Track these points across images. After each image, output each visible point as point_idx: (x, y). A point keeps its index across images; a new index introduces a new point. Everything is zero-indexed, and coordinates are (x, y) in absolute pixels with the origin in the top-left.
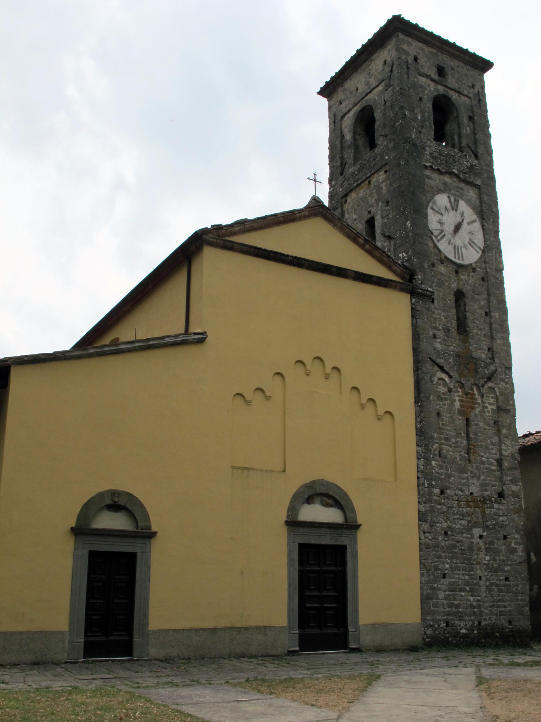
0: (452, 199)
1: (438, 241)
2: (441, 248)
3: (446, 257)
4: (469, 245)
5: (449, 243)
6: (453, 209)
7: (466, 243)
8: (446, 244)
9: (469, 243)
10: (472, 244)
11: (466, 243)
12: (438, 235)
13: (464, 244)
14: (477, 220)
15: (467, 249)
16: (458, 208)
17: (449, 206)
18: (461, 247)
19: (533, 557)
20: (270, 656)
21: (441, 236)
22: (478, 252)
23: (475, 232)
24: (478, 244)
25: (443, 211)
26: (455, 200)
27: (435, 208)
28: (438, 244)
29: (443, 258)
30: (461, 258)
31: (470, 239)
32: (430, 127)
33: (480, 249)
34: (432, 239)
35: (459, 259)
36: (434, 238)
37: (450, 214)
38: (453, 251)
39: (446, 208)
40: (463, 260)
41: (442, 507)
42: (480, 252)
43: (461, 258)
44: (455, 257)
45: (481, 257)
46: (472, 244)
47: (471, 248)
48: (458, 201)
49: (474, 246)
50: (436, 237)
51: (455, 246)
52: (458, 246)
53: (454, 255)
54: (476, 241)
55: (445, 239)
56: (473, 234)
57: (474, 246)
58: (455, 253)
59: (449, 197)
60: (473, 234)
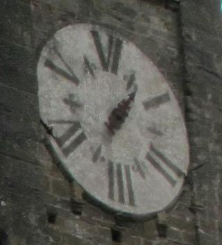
0: (104, 40)
1: (66, 152)
2: (73, 171)
3: (86, 196)
4: (148, 163)
5: (95, 159)
6: (105, 66)
10: (157, 159)
11: (142, 157)
12: (66, 137)
13: (136, 160)
14: (172, 96)
15: (143, 175)
16: (120, 63)
17: (94, 58)
18: (127, 168)
22: (173, 183)
24: (175, 162)
25: (78, 71)
26: (111, 42)
27: (57, 63)
28: (66, 161)
30: (126, 199)
31: (152, 148)
33: (179, 173)
34: (49, 147)
35: (122, 200)
36: (54, 145)
37: (99, 80)
38: (105, 179)
39: (86, 62)
40: (132, 202)
43: (126, 199)
44: (111, 195)
45: (182, 195)
46: (157, 159)
48: (119, 44)
49: (164, 166)
50: (60, 142)
51: (111, 164)
52: (119, 166)
53: (107, 190)
54: (167, 153)
56: (160, 134)
57: (164, 166)
58: (111, 185)
59: (94, 34)
60: (160, 134)
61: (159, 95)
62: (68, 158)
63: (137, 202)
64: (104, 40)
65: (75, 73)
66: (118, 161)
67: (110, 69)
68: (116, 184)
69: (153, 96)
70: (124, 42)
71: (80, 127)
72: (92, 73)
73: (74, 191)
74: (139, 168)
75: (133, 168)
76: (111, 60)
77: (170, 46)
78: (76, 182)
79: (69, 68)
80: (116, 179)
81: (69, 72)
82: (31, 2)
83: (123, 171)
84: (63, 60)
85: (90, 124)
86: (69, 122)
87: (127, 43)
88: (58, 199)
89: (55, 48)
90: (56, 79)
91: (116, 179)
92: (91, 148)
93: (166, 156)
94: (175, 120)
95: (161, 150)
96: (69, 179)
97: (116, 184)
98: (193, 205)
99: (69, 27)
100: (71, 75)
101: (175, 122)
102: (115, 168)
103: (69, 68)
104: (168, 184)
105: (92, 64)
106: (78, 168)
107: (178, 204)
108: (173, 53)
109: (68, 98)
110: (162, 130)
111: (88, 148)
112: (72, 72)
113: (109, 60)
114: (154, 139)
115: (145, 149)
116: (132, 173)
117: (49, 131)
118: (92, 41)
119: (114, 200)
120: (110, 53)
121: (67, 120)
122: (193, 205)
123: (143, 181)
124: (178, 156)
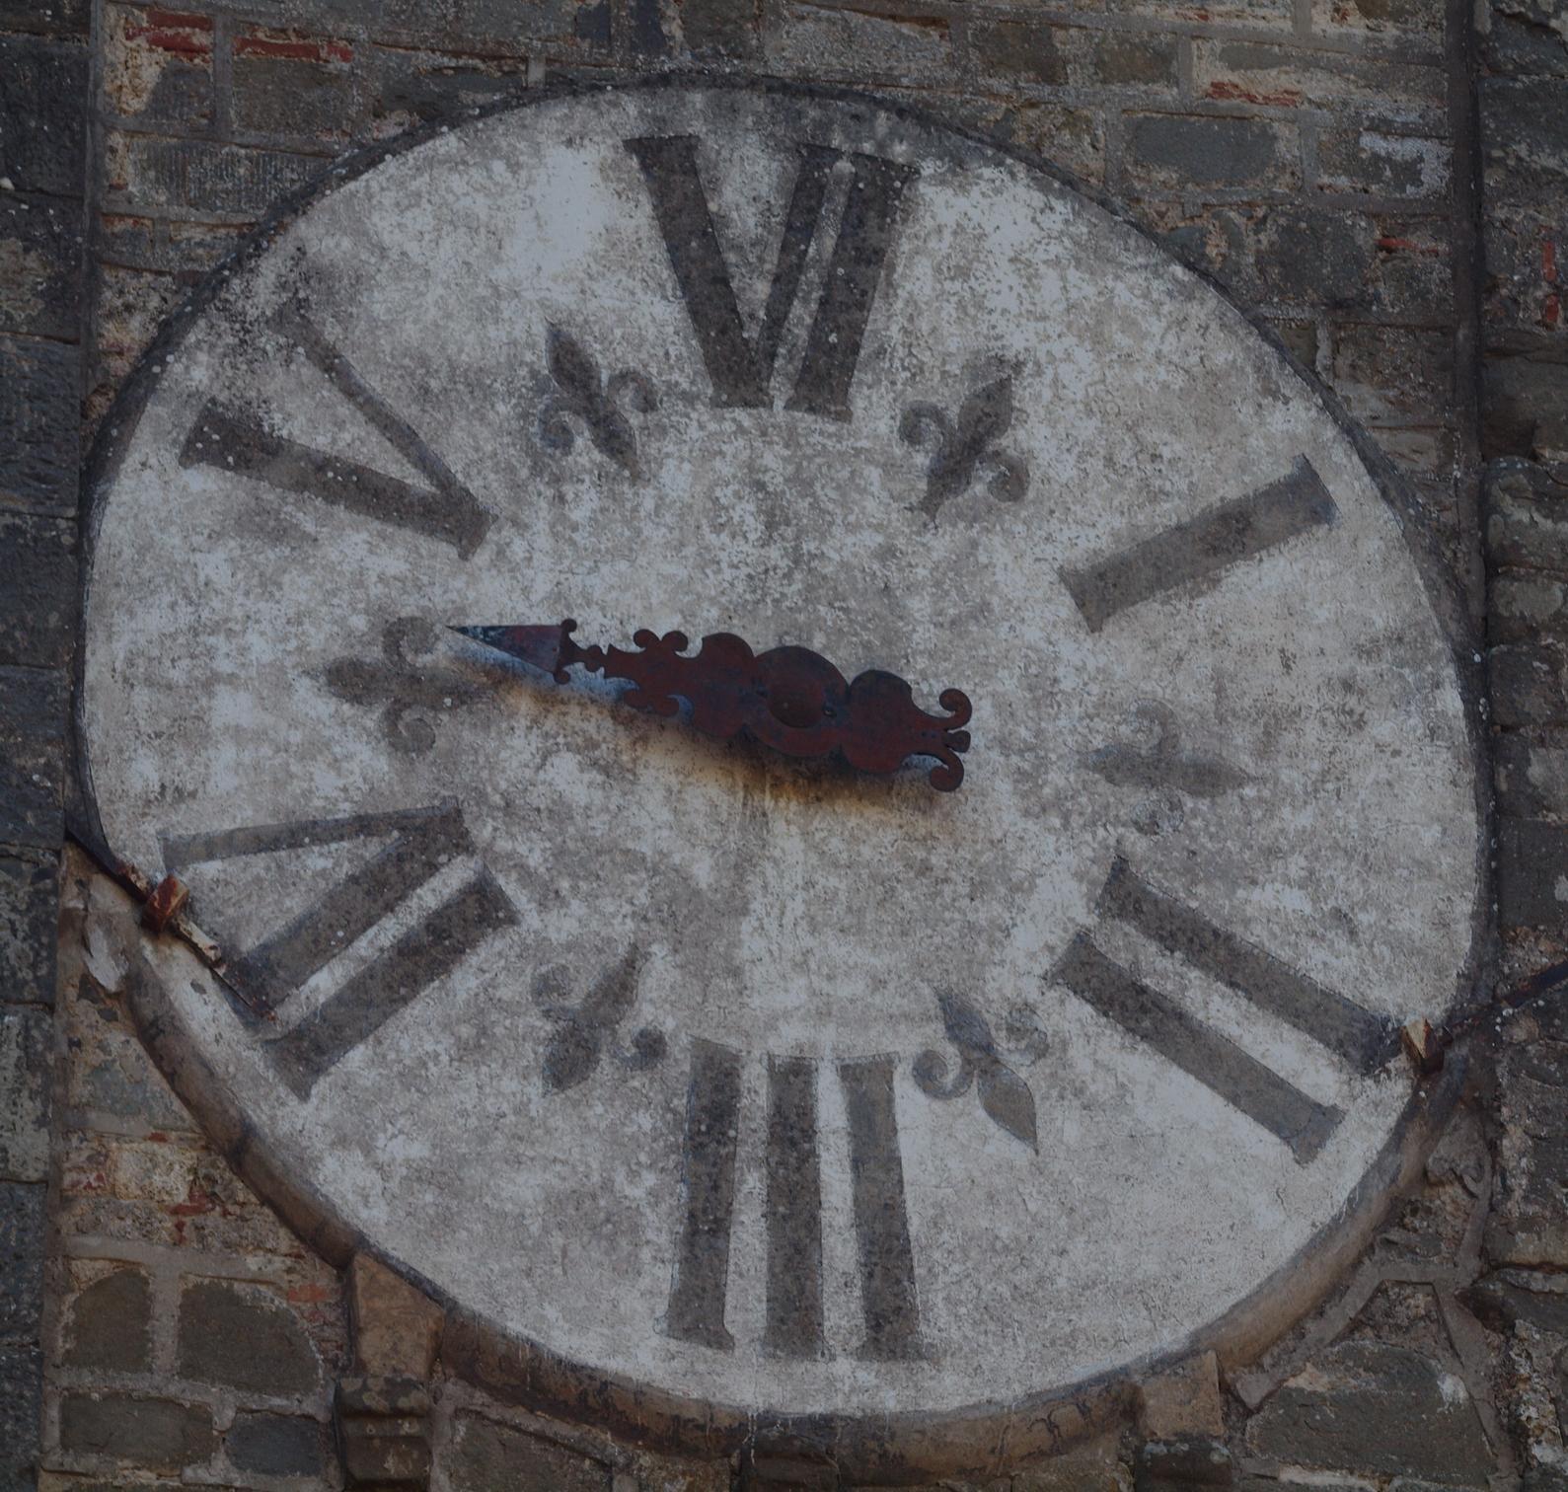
0: (747, 181)
1: (307, 1053)
2: (347, 1185)
3: (464, 1347)
4: (1070, 1015)
5: (568, 1063)
6: (735, 367)
7: (1017, 969)
8: (513, 1086)
9: (1083, 970)
10: (1164, 972)
11: (1017, 969)
12: (314, 940)
13: (957, 1017)
14: (1347, 482)
15: (1015, 1113)
16: (885, 323)
17: (644, 322)
18: (867, 1088)
19: (1545, 768)
20: (1357, 1264)
21: (387, 932)
22: (1302, 1125)
23: (1274, 724)
24: (1330, 965)
25: (476, 450)
26: (803, 201)
27: (306, 417)
28: (295, 1119)
29: (393, 1347)
30: (841, 1312)
31: (1121, 891)
32: (1560, 934)
33: (1368, 1044)
34: (158, 1034)
35: (795, 1325)
36: (203, 1012)
37: (676, 478)
38: (651, 1193)
39: (569, 363)
40: (890, 1329)
41: (1541, 1058)
42: (1369, 1116)
43: (841, 1312)
44: (696, 1315)
45: (1397, 1210)
46: (1164, 972)
47: (1141, 1064)
48: (882, 195)
49: (1219, 1009)
50: (251, 984)
51: (717, 1077)
52: (793, 1075)
53: (663, 1276)
54: (1269, 910)
55: (483, 971)
56: (1210, 778)
57: (1219, 1009)
58: (704, 1230)
59: (667, 168)
60: (1210, 778)
61: (1232, 491)
62: (321, 1087)
63: (940, 1315)
64: (747, 181)
65: (455, 464)
66: (784, 1042)
67: (780, 390)
68: (750, 1238)
69: (1168, 513)
70: (928, 168)
71: (462, 844)
72: (613, 440)
73: (595, 649)
74: (979, 1055)
75: (926, 1072)
76: (802, 314)
77: (1382, 127)
78: (382, 1259)
79: (403, 436)
80: (752, 1184)
81: (391, 465)
82: (110, 17)
83: (831, 1107)
84: (352, 391)
85: (559, 812)
86: (363, 825)
87: (958, 163)
88: (225, 1417)
89: (294, 317)
90: (280, 533)
91: (752, 1184)
92: (546, 987)
93: (1256, 935)
94: (1367, 651)
95: (1206, 900)
96: (331, 1246)
97: (750, 1238)
98: (1493, 1264)
99: (448, 143)
100: (420, 483)
101: (1365, 670)
102: (756, 1095)
103: (403, 436)
104: (1263, 1144)
105: (623, 378)
106: (405, 1148)
107: (1369, 1276)
108: (1409, 171)
109: (375, 654)
110: (1240, 749)
111: (512, 990)
112: (427, 463)
113: (776, 323)
114: (1149, 826)
115: (1059, 900)
116: (910, 1103)
117: (159, 914)
118: (639, 218)
119: (721, 1341)
120: (785, 283)
121: (345, 810)
122: (1493, 1264)
123: (1018, 1152)
124: (1364, 918)
